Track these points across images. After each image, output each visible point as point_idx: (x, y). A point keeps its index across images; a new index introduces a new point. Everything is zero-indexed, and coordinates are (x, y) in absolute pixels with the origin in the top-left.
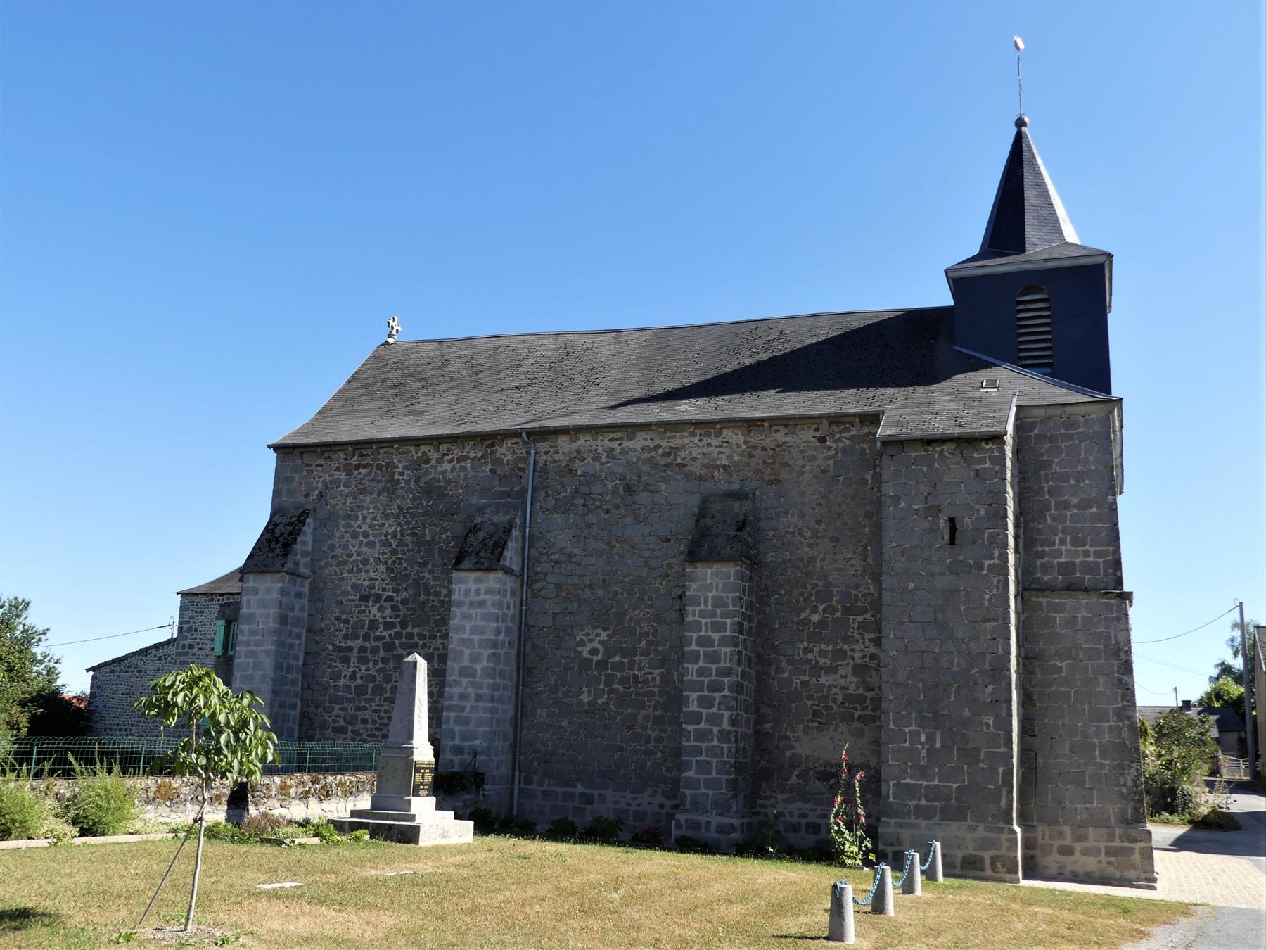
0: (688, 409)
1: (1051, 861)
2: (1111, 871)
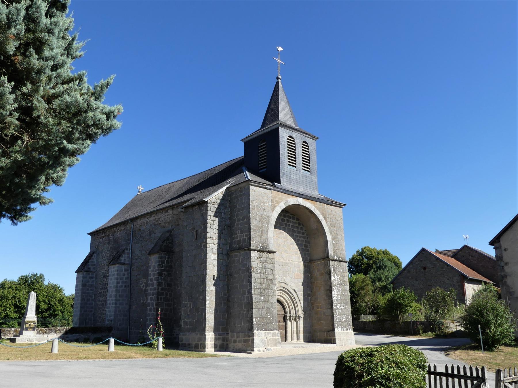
0: (175, 202)
1: (231, 345)
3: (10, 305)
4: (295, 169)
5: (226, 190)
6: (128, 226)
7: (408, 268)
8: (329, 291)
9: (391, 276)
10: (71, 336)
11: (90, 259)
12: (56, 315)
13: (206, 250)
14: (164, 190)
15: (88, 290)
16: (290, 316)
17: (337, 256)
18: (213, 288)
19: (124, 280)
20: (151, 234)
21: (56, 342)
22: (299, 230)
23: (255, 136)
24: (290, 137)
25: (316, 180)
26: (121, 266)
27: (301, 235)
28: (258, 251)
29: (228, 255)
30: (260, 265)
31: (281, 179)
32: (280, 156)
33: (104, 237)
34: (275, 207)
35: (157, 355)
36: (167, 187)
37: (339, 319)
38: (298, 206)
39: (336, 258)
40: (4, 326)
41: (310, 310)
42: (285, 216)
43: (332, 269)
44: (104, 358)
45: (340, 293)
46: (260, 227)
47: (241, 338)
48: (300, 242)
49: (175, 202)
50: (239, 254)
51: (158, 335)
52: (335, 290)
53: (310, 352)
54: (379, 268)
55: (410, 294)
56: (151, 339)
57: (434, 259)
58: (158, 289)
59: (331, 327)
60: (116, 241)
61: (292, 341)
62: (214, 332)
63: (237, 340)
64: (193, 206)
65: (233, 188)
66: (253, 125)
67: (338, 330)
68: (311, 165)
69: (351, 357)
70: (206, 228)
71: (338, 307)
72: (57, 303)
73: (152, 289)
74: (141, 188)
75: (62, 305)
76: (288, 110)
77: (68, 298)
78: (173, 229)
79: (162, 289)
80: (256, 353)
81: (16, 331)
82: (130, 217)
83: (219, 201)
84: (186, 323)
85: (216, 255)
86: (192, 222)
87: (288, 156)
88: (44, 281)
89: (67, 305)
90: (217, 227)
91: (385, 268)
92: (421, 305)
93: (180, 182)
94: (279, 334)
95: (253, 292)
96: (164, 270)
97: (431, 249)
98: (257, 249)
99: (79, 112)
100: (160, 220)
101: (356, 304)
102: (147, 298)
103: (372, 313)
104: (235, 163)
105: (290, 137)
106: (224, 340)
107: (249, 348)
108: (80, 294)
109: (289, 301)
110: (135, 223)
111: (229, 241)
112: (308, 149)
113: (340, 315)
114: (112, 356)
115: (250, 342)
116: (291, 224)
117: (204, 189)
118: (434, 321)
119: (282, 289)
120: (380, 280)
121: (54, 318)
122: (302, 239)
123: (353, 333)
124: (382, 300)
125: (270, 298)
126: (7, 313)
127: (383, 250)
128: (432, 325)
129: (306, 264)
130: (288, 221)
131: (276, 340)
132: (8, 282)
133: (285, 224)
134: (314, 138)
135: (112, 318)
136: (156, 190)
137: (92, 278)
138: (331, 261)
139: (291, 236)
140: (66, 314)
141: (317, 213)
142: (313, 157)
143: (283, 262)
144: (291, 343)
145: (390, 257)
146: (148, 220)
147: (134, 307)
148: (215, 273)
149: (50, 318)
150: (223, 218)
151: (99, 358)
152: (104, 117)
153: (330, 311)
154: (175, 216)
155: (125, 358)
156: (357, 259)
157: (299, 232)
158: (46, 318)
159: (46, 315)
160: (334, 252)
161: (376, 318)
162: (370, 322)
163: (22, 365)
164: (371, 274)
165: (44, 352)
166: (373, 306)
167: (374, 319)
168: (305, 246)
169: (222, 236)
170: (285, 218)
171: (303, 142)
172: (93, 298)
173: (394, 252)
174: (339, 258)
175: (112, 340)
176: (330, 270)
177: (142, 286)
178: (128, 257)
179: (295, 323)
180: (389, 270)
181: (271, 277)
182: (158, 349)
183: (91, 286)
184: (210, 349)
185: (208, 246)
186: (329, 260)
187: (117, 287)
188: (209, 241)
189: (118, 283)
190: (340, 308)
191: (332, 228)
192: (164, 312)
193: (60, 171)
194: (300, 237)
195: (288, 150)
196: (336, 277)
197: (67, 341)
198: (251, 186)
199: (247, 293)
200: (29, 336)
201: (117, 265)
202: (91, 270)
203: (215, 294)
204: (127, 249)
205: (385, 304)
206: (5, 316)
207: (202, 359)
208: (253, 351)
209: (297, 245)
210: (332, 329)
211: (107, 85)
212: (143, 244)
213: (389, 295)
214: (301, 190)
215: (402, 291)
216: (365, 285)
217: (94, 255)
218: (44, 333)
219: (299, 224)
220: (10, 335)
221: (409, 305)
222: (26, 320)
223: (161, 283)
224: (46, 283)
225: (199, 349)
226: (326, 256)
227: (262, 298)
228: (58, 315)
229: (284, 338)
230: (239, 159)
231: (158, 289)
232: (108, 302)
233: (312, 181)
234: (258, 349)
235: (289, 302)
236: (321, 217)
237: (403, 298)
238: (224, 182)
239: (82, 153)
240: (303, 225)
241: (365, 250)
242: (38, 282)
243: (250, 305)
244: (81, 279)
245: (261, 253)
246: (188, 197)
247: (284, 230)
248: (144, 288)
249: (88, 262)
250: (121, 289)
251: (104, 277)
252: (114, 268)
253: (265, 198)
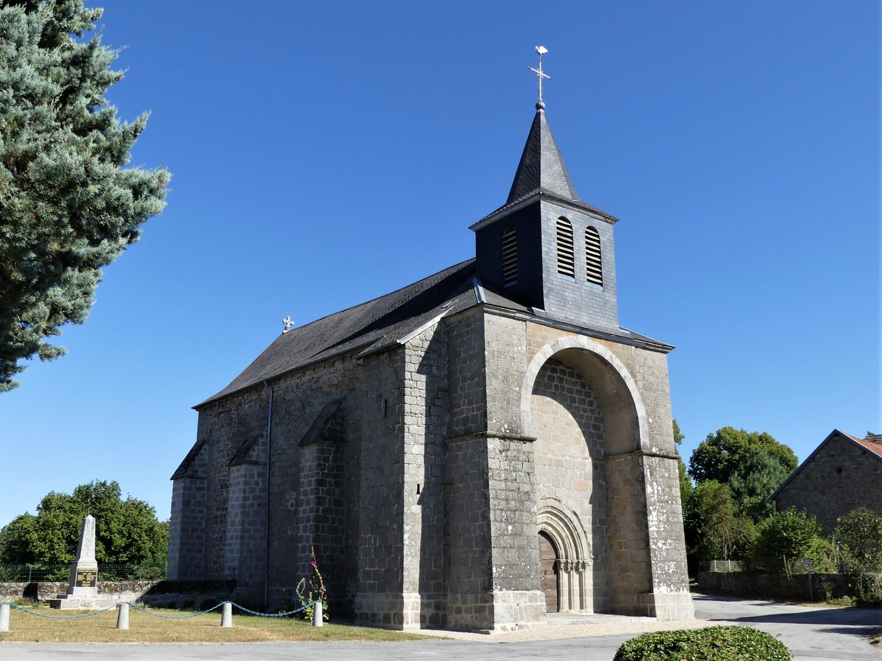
0: (348, 346)
1: (452, 618)
2: (477, 623)
3: (59, 539)
4: (573, 280)
5: (439, 323)
6: (263, 393)
7: (806, 470)
8: (643, 513)
9: (775, 486)
10: (161, 596)
11: (196, 454)
12: (143, 557)
13: (403, 437)
14: (331, 325)
15: (193, 511)
16: (567, 563)
17: (656, 446)
18: (417, 509)
19: (258, 493)
20: (304, 407)
21: (126, 610)
22: (583, 397)
23: (495, 219)
24: (562, 218)
25: (614, 300)
26: (251, 467)
27: (586, 406)
28: (500, 438)
29: (445, 446)
30: (504, 465)
31: (545, 299)
32: (543, 256)
33: (221, 413)
34: (533, 353)
35: (308, 636)
36: (336, 318)
37: (663, 569)
38: (578, 352)
39: (654, 450)
40: (50, 577)
41: (606, 552)
42: (554, 371)
43: (647, 473)
44: (210, 640)
45: (663, 518)
46: (504, 393)
47: (470, 604)
48: (584, 421)
49: (348, 346)
50: (464, 443)
51: (315, 598)
52: (654, 514)
53: (602, 633)
54: (750, 469)
55: (808, 522)
56: (303, 603)
57: (859, 452)
58: (318, 510)
59: (646, 584)
60: (242, 421)
61: (572, 611)
62: (420, 592)
63: (463, 607)
64: (378, 353)
65: (453, 320)
66: (493, 199)
67: (660, 592)
68: (603, 271)
69: (635, 651)
70: (403, 395)
71: (660, 545)
72: (143, 535)
73: (307, 509)
74: (290, 322)
75: (152, 539)
76: (558, 168)
77: (163, 526)
78: (345, 398)
79: (324, 511)
80: (498, 633)
81: (62, 587)
82: (268, 377)
83: (426, 345)
84: (367, 574)
85: (423, 447)
86: (377, 384)
87: (559, 255)
88: (120, 494)
89: (162, 540)
90: (423, 393)
91: (762, 469)
92: (831, 543)
93: (359, 309)
94: (543, 598)
95: (491, 515)
96: (328, 475)
97: (856, 433)
98: (499, 434)
99: (71, 185)
100: (321, 380)
101: (702, 539)
102: (298, 528)
103: (734, 557)
104: (459, 272)
105: (562, 218)
106: (438, 607)
107: (485, 624)
108: (180, 519)
109: (565, 533)
110: (276, 388)
111: (447, 419)
112: (599, 242)
113: (663, 562)
114: (228, 636)
115: (487, 612)
116: (567, 386)
117: (401, 321)
118: (856, 574)
119: (549, 509)
120: (752, 492)
121: (139, 563)
122: (589, 414)
123: (690, 595)
124: (753, 532)
125: (525, 527)
126: (54, 554)
127: (760, 433)
128: (852, 582)
129: (598, 462)
130: (561, 380)
131: (537, 609)
132: (56, 497)
133: (556, 386)
134: (609, 219)
135: (236, 563)
136: (315, 324)
137: (200, 489)
138: (645, 457)
139: (568, 407)
140: (159, 555)
141: (617, 363)
142: (609, 256)
143: (551, 459)
144: (568, 615)
145: (774, 448)
146: (298, 381)
147: (275, 543)
148: (421, 479)
149: (133, 563)
150: (434, 376)
151: (201, 640)
152: (129, 192)
153: (643, 552)
154: (347, 373)
155: (249, 641)
156: (708, 452)
157: (582, 402)
158: (124, 562)
159: (123, 557)
160: (652, 439)
161: (743, 567)
162: (728, 574)
163: (58, 652)
164: (735, 481)
165: (105, 627)
166: (736, 543)
167: (738, 570)
168: (596, 427)
169: (434, 410)
170: (555, 375)
171: (588, 228)
172: (204, 526)
173: (781, 438)
174: (660, 450)
175: (228, 606)
176: (643, 473)
177: (289, 504)
178: (265, 450)
179: (575, 577)
180: (769, 472)
181: (526, 488)
182: (314, 624)
183: (200, 503)
184: (411, 621)
185: (406, 430)
186: (642, 454)
187: (244, 506)
188: (408, 420)
189: (246, 499)
190: (664, 547)
191: (646, 393)
192: (328, 553)
193: (80, 295)
194: (585, 411)
195: (559, 244)
196: (656, 487)
197: (153, 606)
198: (486, 315)
199: (480, 519)
200: (84, 597)
201: (244, 466)
202: (200, 474)
203: (420, 521)
204: (262, 436)
205: (758, 541)
206: (50, 559)
207: (393, 644)
208: (493, 628)
209: (581, 427)
210: (648, 588)
211: (136, 131)
212: (290, 427)
213: (766, 524)
214: (584, 320)
215: (790, 515)
216: (719, 503)
217: (205, 446)
218: (112, 590)
219: (583, 386)
220: (53, 595)
221: (805, 542)
222: (78, 567)
223: (324, 498)
224: (123, 498)
225: (392, 624)
226: (635, 446)
227: (510, 528)
228: (146, 557)
229: (555, 605)
230: (467, 264)
231: (318, 510)
232: (229, 534)
233: (606, 303)
234: (502, 625)
235: (563, 535)
236: (624, 373)
237: (794, 529)
238: (438, 308)
239: (107, 261)
240: (590, 388)
241: (723, 434)
242: (109, 497)
243: (486, 542)
244: (181, 491)
245: (507, 442)
246: (372, 336)
247: (554, 397)
248: (293, 509)
249: (194, 460)
250: (251, 510)
251: (222, 488)
252: (238, 470)
253: (515, 337)
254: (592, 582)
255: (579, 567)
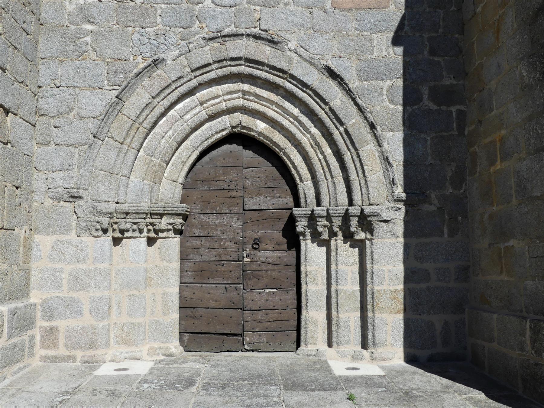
119: (244, 69)
235: (305, 140)
254: (400, 269)
255: (356, 228)
